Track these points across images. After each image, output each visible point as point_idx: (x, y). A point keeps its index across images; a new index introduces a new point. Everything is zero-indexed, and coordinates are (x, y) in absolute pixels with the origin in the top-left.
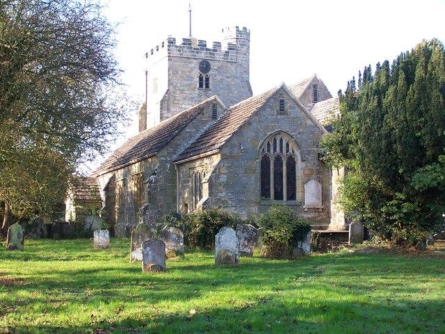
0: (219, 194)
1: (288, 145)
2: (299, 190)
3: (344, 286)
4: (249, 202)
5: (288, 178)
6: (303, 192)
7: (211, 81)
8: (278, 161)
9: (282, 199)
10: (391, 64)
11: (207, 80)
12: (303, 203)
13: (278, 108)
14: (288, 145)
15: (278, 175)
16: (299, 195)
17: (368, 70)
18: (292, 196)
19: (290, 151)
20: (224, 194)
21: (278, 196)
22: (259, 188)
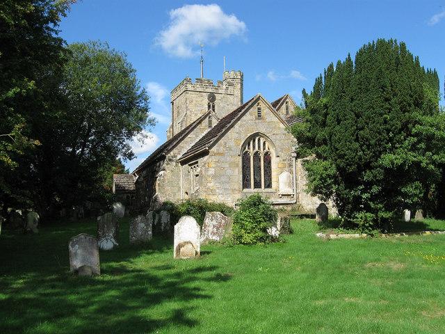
0: (209, 184)
1: (264, 144)
2: (274, 180)
3: (170, 268)
4: (233, 190)
5: (265, 171)
6: (278, 181)
7: (216, 107)
8: (256, 154)
9: (260, 187)
10: (353, 59)
11: (214, 107)
12: (277, 190)
13: (257, 114)
14: (264, 144)
15: (257, 169)
16: (274, 185)
17: (331, 66)
18: (269, 185)
19: (267, 149)
20: (212, 184)
21: (257, 185)
22: (230, 113)
